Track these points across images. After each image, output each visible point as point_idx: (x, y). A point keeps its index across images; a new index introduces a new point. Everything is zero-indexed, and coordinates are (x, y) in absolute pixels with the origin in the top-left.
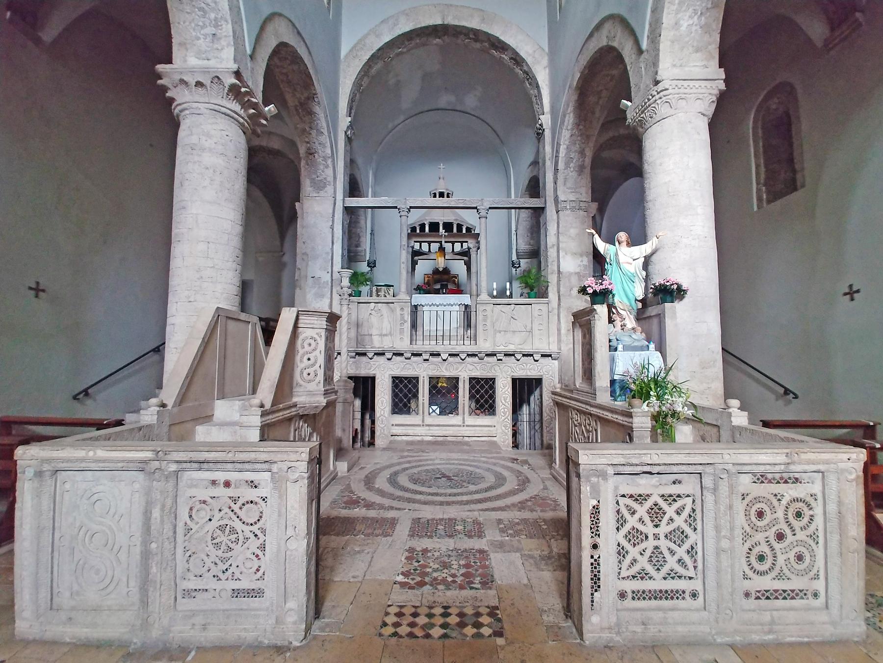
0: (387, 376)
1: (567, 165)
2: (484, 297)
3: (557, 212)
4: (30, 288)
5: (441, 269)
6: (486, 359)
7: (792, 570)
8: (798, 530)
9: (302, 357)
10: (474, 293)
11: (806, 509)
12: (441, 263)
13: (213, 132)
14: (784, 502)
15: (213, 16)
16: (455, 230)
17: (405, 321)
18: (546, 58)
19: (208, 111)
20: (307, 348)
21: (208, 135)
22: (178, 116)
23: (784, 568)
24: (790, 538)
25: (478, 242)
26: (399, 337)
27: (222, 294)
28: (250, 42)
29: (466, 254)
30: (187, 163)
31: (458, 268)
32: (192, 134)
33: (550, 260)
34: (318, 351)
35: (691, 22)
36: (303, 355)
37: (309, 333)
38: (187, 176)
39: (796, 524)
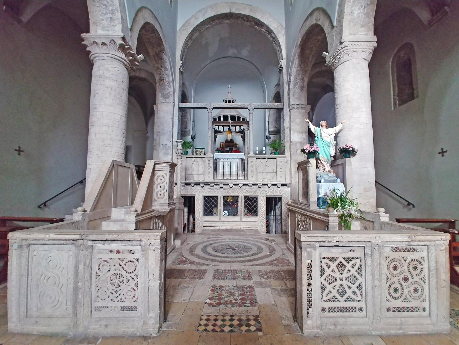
0: (201, 195)
1: (295, 86)
2: (252, 154)
3: (290, 110)
4: (16, 150)
5: (229, 140)
6: (253, 187)
7: (412, 297)
8: (415, 276)
9: (157, 186)
10: (247, 152)
11: (419, 265)
12: (229, 137)
13: (111, 69)
14: (408, 261)
15: (110, 8)
16: (236, 120)
17: (211, 167)
18: (284, 30)
19: (108, 58)
20: (160, 181)
21: (108, 71)
22: (92, 60)
23: (408, 295)
24: (411, 280)
25: (249, 126)
26: (207, 175)
27: (115, 153)
28: (130, 22)
29: (242, 132)
30: (97, 85)
31: (238, 139)
32: (100, 70)
33: (286, 135)
34: (165, 183)
35: (359, 11)
36: (158, 185)
37: (160, 173)
38: (97, 92)
39: (414, 273)
